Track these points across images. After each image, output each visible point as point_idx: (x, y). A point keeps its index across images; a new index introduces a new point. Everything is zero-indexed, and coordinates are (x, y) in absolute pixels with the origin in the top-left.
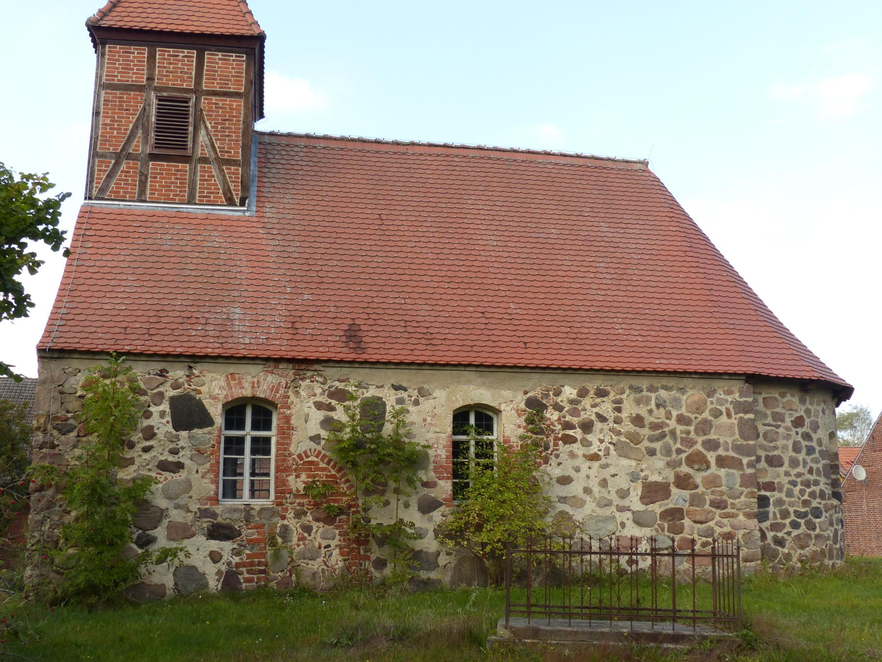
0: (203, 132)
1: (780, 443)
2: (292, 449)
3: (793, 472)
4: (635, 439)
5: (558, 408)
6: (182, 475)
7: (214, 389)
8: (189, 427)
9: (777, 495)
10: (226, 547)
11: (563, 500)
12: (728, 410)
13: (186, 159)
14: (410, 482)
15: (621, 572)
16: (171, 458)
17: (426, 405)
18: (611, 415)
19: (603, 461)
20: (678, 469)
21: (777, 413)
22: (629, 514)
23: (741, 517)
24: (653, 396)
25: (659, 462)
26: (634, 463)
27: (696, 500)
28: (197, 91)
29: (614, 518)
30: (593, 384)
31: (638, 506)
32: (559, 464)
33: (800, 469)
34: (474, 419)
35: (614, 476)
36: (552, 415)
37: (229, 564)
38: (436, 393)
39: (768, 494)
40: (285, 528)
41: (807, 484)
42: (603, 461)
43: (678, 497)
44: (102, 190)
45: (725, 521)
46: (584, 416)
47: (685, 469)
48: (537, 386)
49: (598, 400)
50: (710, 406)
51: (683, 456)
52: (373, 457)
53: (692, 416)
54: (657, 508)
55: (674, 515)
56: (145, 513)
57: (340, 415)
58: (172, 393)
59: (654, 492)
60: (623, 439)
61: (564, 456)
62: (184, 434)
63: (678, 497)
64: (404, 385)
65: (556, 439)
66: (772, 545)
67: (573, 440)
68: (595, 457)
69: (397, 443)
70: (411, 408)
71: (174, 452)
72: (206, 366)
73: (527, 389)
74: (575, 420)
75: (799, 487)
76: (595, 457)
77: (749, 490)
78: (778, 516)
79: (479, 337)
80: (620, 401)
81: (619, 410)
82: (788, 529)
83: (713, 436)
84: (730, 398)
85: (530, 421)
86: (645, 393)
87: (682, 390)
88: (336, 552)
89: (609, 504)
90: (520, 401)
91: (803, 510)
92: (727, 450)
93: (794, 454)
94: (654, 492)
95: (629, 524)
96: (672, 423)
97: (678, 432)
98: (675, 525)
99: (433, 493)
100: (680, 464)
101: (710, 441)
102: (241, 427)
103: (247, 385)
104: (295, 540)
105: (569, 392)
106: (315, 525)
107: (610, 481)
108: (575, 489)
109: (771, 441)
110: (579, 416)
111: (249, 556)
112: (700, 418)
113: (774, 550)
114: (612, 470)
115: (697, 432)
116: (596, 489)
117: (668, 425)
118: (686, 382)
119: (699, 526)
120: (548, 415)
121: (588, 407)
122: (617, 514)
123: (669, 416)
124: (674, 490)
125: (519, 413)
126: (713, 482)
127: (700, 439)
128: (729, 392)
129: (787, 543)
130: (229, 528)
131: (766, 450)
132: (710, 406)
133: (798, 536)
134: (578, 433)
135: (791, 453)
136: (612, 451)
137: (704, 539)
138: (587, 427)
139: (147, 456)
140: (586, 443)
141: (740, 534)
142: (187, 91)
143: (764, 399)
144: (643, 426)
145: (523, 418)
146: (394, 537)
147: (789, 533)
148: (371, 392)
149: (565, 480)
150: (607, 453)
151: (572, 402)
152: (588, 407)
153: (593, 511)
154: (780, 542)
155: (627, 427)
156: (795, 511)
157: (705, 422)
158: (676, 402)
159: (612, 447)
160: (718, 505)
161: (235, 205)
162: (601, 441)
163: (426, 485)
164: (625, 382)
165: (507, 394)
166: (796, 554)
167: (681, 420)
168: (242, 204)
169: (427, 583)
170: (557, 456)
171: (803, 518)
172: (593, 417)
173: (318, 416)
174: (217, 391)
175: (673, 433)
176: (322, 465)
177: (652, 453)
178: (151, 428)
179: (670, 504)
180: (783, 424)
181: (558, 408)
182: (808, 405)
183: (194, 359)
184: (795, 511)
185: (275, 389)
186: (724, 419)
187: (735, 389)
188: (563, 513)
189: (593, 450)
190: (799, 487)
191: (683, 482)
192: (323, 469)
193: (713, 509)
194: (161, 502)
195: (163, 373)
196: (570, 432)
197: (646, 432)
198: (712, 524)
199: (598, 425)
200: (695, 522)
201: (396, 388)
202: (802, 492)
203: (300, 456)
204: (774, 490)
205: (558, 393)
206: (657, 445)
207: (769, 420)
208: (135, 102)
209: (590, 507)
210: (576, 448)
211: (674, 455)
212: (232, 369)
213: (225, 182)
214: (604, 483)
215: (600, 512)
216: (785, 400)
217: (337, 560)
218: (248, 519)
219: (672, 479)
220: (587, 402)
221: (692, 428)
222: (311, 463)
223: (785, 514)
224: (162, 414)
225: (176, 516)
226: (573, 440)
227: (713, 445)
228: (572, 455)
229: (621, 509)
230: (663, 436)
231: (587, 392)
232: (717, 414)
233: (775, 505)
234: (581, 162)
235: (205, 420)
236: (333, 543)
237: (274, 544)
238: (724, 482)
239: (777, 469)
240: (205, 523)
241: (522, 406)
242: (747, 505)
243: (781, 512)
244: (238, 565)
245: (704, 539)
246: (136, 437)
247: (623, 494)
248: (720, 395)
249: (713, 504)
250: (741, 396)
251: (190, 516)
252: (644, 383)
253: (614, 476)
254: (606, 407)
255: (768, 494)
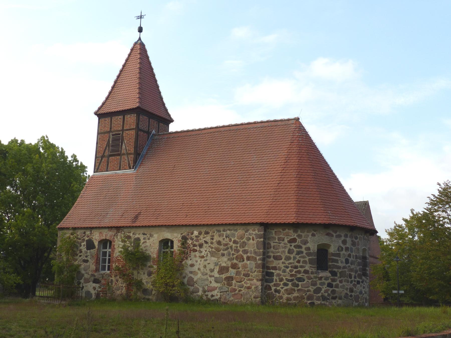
0: (124, 144)
1: (280, 250)
2: (114, 255)
3: (287, 262)
4: (218, 250)
5: (192, 239)
6: (88, 264)
7: (96, 237)
8: (90, 249)
9: (278, 272)
10: (97, 285)
11: (191, 272)
12: (253, 238)
13: (119, 155)
14: (145, 266)
15: (209, 300)
16: (86, 259)
17: (152, 239)
18: (209, 241)
19: (205, 258)
20: (232, 261)
21: (281, 237)
22: (213, 278)
23: (255, 281)
24: (225, 233)
25: (225, 259)
26: (216, 259)
27: (238, 273)
28: (123, 130)
29: (208, 279)
30: (203, 230)
31: (217, 275)
32: (191, 259)
33: (291, 261)
34: (166, 244)
35: (209, 264)
36: (190, 242)
37: (98, 291)
38: (154, 236)
39: (274, 271)
40: (112, 280)
41: (296, 267)
42: (205, 258)
43: (232, 272)
44: (98, 169)
45: (248, 282)
46: (200, 241)
47: (235, 261)
48: (185, 231)
49: (205, 236)
50: (246, 236)
51: (235, 256)
52: (137, 258)
53: (239, 240)
54: (224, 276)
55: (229, 279)
56: (80, 275)
57: (128, 244)
58: (87, 239)
59: (223, 270)
60: (213, 250)
61: (192, 257)
62: (89, 251)
63: (232, 272)
64: (146, 233)
65: (190, 250)
66: (274, 292)
67: (196, 251)
68: (203, 257)
69: (143, 253)
70: (147, 241)
71: (86, 257)
72: (95, 230)
73: (182, 233)
74: (197, 243)
75: (290, 268)
76: (203, 257)
77: (258, 270)
78: (278, 280)
79: (312, 203)
80: (213, 236)
81: (212, 239)
82: (282, 286)
83: (246, 248)
84: (254, 233)
85: (183, 244)
86: (222, 232)
87: (236, 230)
88: (124, 288)
89: (207, 274)
90: (179, 237)
91: (291, 278)
92: (251, 253)
93: (288, 255)
94: (223, 270)
95: (213, 282)
96: (231, 243)
97: (233, 247)
98: (229, 283)
99: (151, 270)
100: (233, 259)
101: (245, 250)
102: (107, 249)
103: (104, 235)
104: (114, 284)
105: (196, 233)
106: (119, 279)
107: (207, 266)
108: (195, 268)
109: (277, 249)
110: (198, 242)
111: (103, 289)
112: (242, 241)
113: (274, 294)
114: (208, 262)
115: (240, 247)
116: (202, 269)
117: (230, 244)
118: (236, 228)
119: (239, 283)
120: (188, 242)
121: (202, 238)
122: (209, 278)
123: (230, 240)
124: (230, 269)
125: (179, 241)
126: (245, 266)
127: (241, 250)
128: (254, 230)
129: (281, 292)
130: (98, 280)
131: (273, 253)
132: (246, 236)
133: (287, 289)
134: (197, 248)
135: (287, 254)
136: (209, 255)
137: (240, 289)
138: (201, 246)
139: (80, 258)
140: (201, 252)
141: (253, 287)
142: (120, 131)
143: (275, 232)
144: (221, 245)
145: (180, 243)
146: (139, 284)
147: (282, 288)
148: (137, 236)
149: (192, 265)
150: (207, 256)
151: (196, 237)
152: (202, 238)
153: (200, 277)
154: (279, 292)
155: (215, 245)
156: (286, 279)
157: (244, 242)
158: (233, 235)
159: (209, 253)
160: (247, 275)
161: (131, 169)
162: (206, 251)
163: (149, 267)
164: (215, 229)
165: (175, 235)
166: (285, 296)
167: (235, 242)
168: (133, 169)
169: (148, 300)
170: (190, 257)
171: (290, 282)
172: (203, 242)
173: (122, 244)
174: (97, 238)
175: (231, 247)
176: (122, 260)
177: (223, 255)
178: (81, 249)
179: (228, 275)
180: (283, 242)
181: (192, 239)
182: (299, 232)
183: (91, 228)
184: (286, 279)
185: (111, 236)
186: (251, 241)
187: (256, 229)
188: (191, 277)
189: (202, 254)
190: (290, 268)
191: (234, 266)
192: (122, 262)
193: (244, 277)
194: (83, 272)
195: (85, 233)
196: (195, 248)
197: (222, 247)
198: (243, 283)
199: (205, 245)
200: (237, 282)
201: (144, 234)
202: (291, 271)
203: (116, 258)
204: (276, 270)
205: (192, 234)
206: (225, 252)
207: (277, 241)
208: (106, 137)
209: (199, 275)
210: (197, 254)
211: (231, 256)
212: (101, 231)
213: (129, 161)
214: (205, 267)
215: (203, 277)
216: (285, 232)
217: (124, 291)
218: (103, 277)
219: (230, 265)
220: (201, 237)
221: (238, 245)
222: (119, 260)
223: (281, 280)
224: (84, 245)
225: (86, 276)
226: (196, 251)
227: (245, 252)
228: (195, 256)
229: (211, 276)
230: (228, 248)
231: (202, 233)
232: (249, 239)
233: (276, 276)
234: (270, 124)
235: (94, 247)
236: (124, 285)
237: (109, 285)
238: (249, 266)
239: (279, 261)
240: (92, 278)
241: (180, 239)
242: (257, 276)
243: (279, 278)
244: (100, 291)
245: (240, 289)
246: (78, 252)
247: (212, 271)
248: (251, 231)
249: (244, 275)
250: (258, 232)
251: (89, 276)
252: (221, 229)
253: (209, 264)
254: (208, 238)
255: (274, 271)
